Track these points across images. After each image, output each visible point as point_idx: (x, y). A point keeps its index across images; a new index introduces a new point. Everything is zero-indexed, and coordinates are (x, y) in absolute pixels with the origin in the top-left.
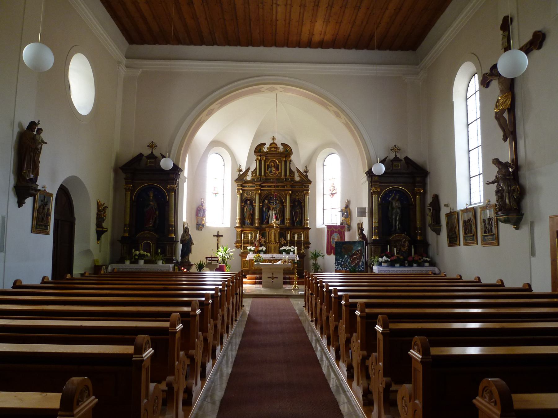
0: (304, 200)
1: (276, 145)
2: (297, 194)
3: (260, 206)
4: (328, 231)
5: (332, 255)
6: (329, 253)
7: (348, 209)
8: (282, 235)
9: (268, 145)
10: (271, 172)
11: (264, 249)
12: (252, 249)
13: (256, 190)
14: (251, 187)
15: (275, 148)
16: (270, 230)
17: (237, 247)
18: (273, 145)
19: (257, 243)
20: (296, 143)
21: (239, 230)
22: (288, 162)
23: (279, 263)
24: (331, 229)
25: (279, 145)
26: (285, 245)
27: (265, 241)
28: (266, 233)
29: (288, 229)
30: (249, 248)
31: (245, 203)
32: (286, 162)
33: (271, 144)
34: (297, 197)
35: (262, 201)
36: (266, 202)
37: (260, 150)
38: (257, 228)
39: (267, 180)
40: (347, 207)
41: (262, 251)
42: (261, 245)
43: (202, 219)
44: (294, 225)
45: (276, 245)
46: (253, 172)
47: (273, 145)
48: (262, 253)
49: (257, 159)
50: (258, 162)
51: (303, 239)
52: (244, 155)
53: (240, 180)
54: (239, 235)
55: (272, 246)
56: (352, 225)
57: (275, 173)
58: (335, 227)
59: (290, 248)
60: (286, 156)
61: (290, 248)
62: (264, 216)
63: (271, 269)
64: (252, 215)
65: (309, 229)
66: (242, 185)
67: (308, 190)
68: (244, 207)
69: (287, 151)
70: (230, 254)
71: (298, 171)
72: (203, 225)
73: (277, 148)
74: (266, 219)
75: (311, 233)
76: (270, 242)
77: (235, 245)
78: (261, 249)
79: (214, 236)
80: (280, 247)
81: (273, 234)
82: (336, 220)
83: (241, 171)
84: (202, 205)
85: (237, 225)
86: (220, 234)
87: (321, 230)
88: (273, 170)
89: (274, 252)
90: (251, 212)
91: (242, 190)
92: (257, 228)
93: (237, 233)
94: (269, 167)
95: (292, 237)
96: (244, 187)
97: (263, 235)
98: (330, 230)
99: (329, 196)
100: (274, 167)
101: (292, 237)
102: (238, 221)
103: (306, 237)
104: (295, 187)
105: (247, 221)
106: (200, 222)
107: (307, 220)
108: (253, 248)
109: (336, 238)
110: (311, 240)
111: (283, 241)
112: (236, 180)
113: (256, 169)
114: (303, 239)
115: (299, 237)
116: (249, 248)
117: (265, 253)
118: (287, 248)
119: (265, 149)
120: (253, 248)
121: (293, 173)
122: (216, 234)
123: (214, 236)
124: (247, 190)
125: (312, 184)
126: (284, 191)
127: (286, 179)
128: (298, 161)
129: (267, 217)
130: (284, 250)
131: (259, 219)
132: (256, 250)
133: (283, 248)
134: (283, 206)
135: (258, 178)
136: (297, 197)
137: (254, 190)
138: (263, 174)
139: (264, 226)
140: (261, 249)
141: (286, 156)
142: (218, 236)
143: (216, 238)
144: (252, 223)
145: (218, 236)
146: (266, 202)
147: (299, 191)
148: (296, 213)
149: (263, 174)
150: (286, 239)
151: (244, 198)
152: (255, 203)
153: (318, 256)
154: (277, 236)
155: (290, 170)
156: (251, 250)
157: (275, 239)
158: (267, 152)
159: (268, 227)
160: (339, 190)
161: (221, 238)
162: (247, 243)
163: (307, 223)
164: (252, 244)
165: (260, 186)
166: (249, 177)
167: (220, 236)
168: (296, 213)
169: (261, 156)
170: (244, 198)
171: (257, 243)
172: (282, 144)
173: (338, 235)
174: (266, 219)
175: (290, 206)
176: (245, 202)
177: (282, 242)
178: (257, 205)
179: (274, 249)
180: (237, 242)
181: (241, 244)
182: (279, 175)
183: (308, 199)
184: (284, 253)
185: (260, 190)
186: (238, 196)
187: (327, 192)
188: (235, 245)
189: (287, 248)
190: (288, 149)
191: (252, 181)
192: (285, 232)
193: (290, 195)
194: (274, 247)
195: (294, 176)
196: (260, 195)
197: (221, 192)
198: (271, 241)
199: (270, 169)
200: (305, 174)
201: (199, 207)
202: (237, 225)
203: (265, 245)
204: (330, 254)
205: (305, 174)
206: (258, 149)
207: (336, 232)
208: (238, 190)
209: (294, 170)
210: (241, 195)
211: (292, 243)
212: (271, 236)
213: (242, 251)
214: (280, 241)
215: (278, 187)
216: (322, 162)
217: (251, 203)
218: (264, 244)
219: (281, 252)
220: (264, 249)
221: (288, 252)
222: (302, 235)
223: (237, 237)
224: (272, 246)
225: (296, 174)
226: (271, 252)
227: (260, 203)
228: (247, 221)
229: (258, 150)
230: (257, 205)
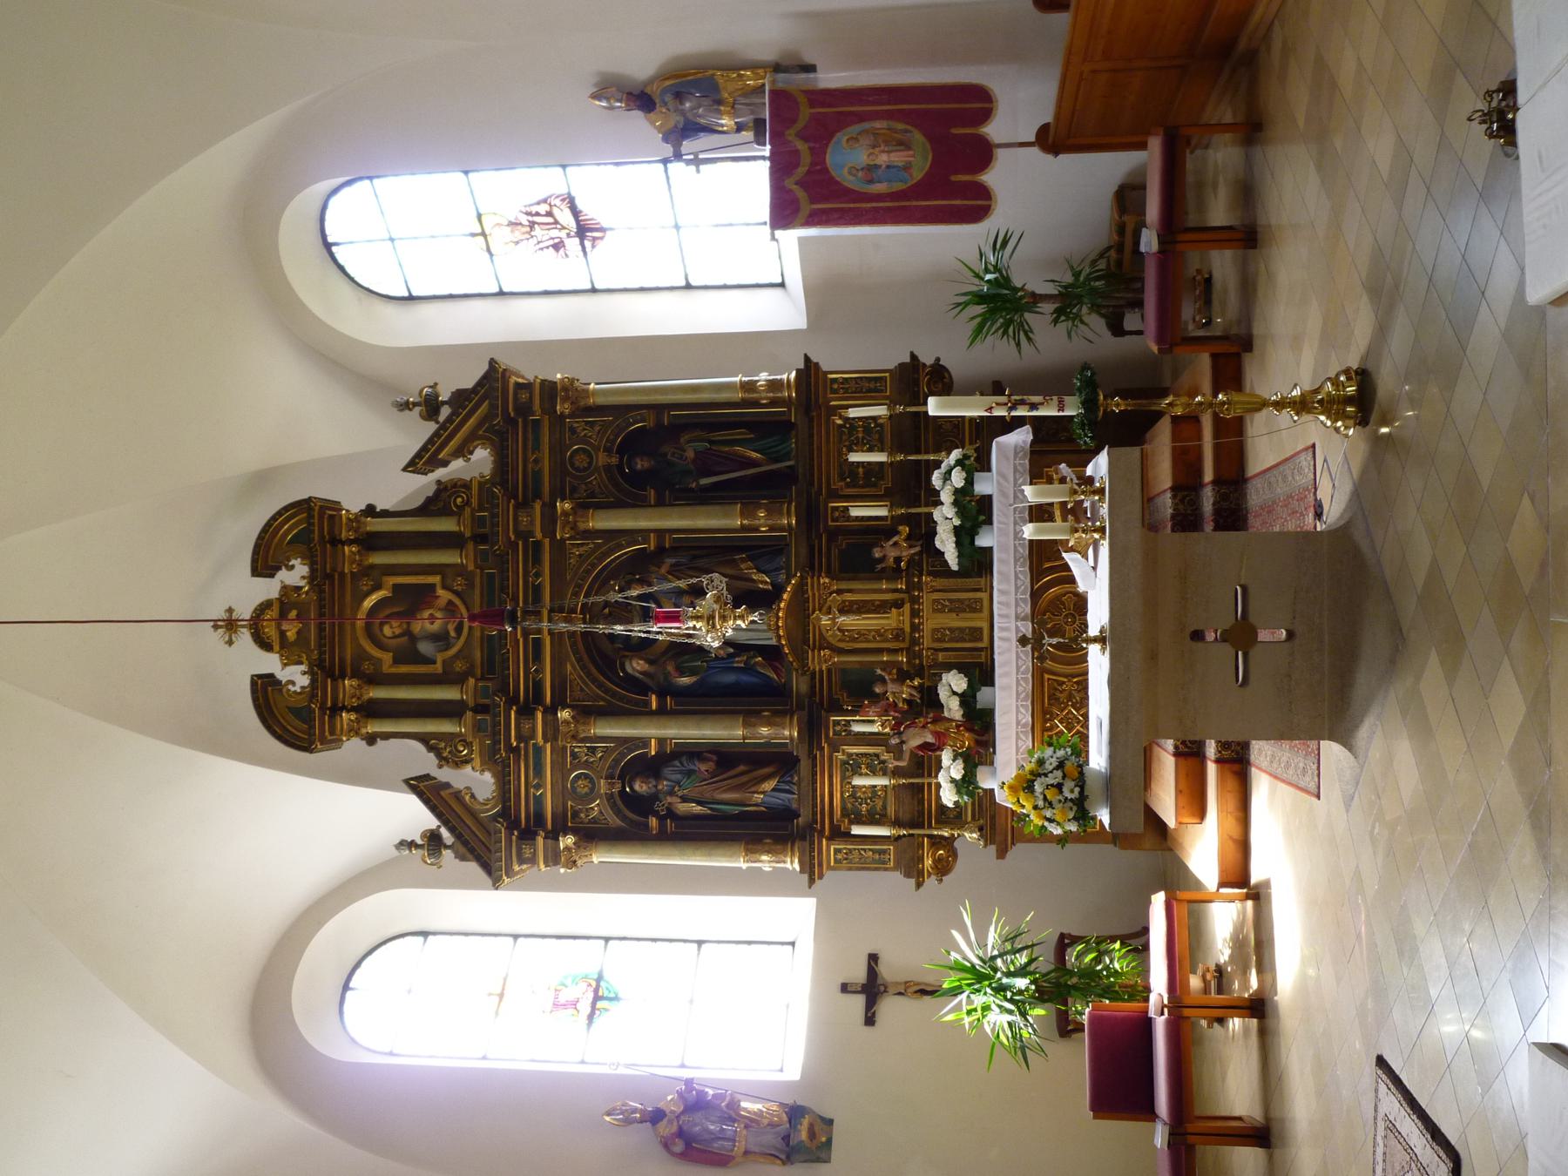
0: (621, 411)
1: (265, 606)
2: (581, 461)
3: (662, 712)
4: (811, 221)
5: (989, 178)
6: (975, 205)
7: (654, 90)
8: (855, 554)
9: (270, 663)
10: (441, 639)
11: (955, 682)
12: (957, 771)
13: (552, 732)
14: (539, 771)
15: (283, 615)
16: (824, 644)
17: (943, 868)
18: (262, 627)
19: (916, 739)
20: (261, 479)
21: (830, 850)
22: (374, 525)
23: (1094, 579)
24: (803, 196)
25: (268, 589)
26: (925, 531)
27: (903, 676)
28: (844, 671)
29: (811, 515)
30: (949, 797)
31: (647, 814)
32: (372, 542)
33: (264, 644)
34: (602, 459)
35: (629, 698)
36: (637, 666)
37: (303, 714)
38: (813, 730)
39: (494, 664)
40: (641, 99)
41: (967, 699)
42: (930, 700)
43: (751, 1122)
44: (789, 477)
45: (927, 599)
46: (443, 760)
47: (262, 627)
48: (983, 695)
49: (354, 731)
50: (373, 727)
51: (880, 411)
52: (357, 810)
53: (485, 838)
54: (871, 858)
55: (932, 622)
56: (769, 56)
57: (450, 609)
58: (781, 169)
59: (946, 496)
60: (336, 542)
61: (946, 496)
62: (730, 678)
63: (1153, 656)
64: (725, 758)
65: (809, 371)
66: (528, 835)
67: (550, 390)
68: (671, 814)
69: (306, 532)
70: (992, 937)
71: (422, 461)
72: (795, 1113)
73: (286, 602)
74: (748, 669)
75: (838, 360)
76: (908, 640)
77: (931, 882)
78: (953, 709)
79: (870, 1021)
80: (942, 569)
81: (850, 621)
82: (742, 180)
83: (433, 841)
84: (656, 1117)
85: (792, 864)
86: (859, 975)
87: (825, 294)
88: (428, 623)
89: (974, 607)
90: (710, 766)
91: (553, 836)
92: (813, 730)
93: (846, 863)
94: (408, 654)
95: (867, 482)
96: (539, 818)
97: (859, 689)
98: (806, 208)
99: (601, 252)
100: (410, 613)
101: (867, 482)
102: (766, 863)
103: (865, 387)
104: (538, 475)
105: (765, 793)
106: (771, 1139)
107: (749, 387)
108: (951, 769)
109: (861, 156)
110: (886, 356)
111: (896, 550)
112: (487, 867)
113: (423, 738)
114: (880, 411)
115: (868, 434)
116: (949, 797)
117: (981, 673)
118: (945, 516)
119: (296, 677)
120: (951, 769)
121: (443, 489)
122: (859, 1001)
123: (870, 1021)
124: (561, 793)
125: (505, 361)
126: (559, 547)
127: (480, 538)
128: (373, 466)
129: (739, 662)
130: (965, 535)
131: (751, 717)
132: (967, 740)
133: (946, 543)
134: (661, 551)
135: (478, 728)
136: (602, 459)
137: (559, 752)
138: (449, 694)
139: (799, 684)
140: (953, 708)
141: (336, 542)
142: (872, 989)
143: (889, 1007)
144: (780, 761)
145: (872, 989)
146: (637, 666)
147: (558, 449)
148: (705, 465)
149: (449, 694)
150: (878, 531)
151: (614, 821)
152: (645, 742)
153: (1004, 281)
154: (862, 591)
155: (428, 508)
156: (966, 784)
157: (881, 608)
158: (310, 672)
159: (802, 658)
160: (533, 183)
161: (885, 971)
162: (916, 810)
163: (774, 385)
164: (925, 762)
165: (526, 712)
166: (478, 782)
167: (872, 973)
168: (705, 465)
169: (336, 709)
170: (614, 821)
171: (916, 739)
172: (264, 562)
173: (842, 137)
174: (748, 669)
175: (660, 503)
176: (641, 806)
177: (907, 552)
178: (655, 732)
179: (958, 608)
180: (914, 871)
181: (921, 838)
182: (459, 583)
183: (600, 384)
184: (983, 541)
185: (551, 711)
186: (600, 857)
187: (569, 269)
188: (931, 882)
189: (945, 516)
190: (289, 530)
191: (500, 761)
192: (834, 534)
193: (583, 507)
194: (939, 608)
195: (466, 485)
196: (586, 712)
197: (588, 957)
198: (898, 635)
199: (425, 648)
200: (445, 412)
201: (666, 1145)
202: (792, 864)
203: (925, 675)
204: (984, 193)
205: (445, 412)
206: (295, 725)
207: (818, 155)
208: (554, 858)
209: (420, 485)
210: (593, 835)
211: (912, 487)
212: (862, 635)
213: (971, 836)
214: (895, 573)
215: (537, 590)
216: (391, 310)
217: (651, 766)
218: (928, 687)
219: (979, 563)
220: (955, 682)
221: (975, 512)
222: (853, 413)
223: (879, 864)
224: (932, 622)
225: (456, 468)
226: (975, 634)
227: (639, 711)
228: (765, 793)
229: (297, 724)
230: (655, 732)
